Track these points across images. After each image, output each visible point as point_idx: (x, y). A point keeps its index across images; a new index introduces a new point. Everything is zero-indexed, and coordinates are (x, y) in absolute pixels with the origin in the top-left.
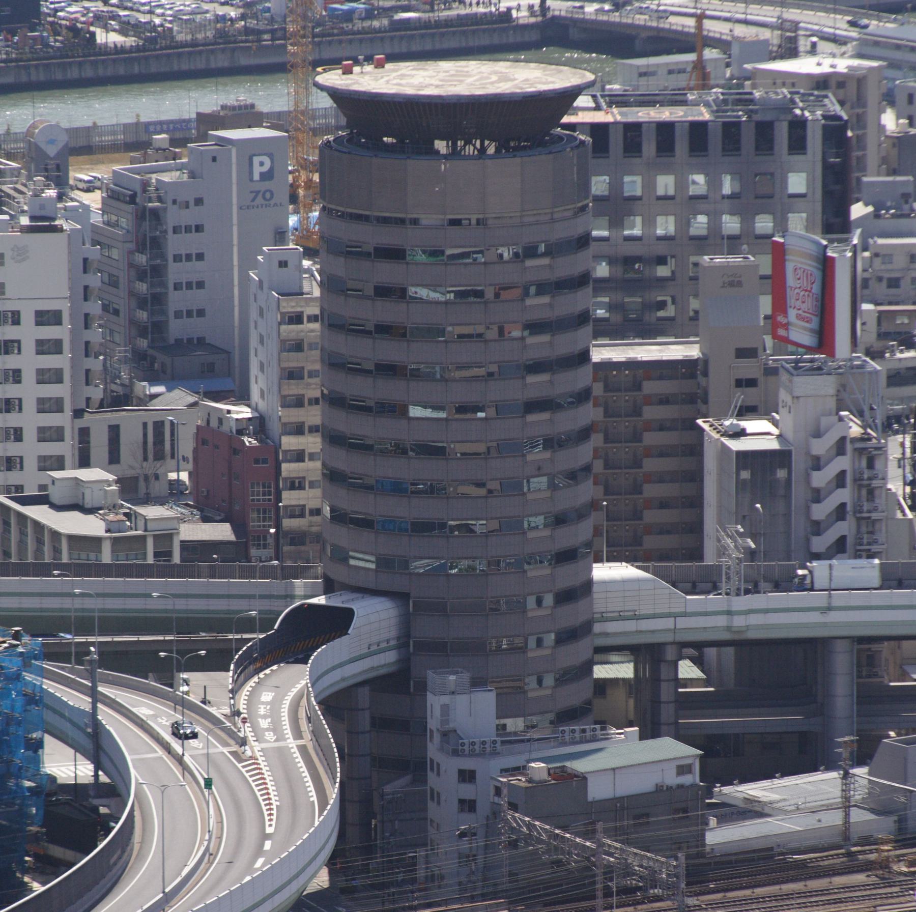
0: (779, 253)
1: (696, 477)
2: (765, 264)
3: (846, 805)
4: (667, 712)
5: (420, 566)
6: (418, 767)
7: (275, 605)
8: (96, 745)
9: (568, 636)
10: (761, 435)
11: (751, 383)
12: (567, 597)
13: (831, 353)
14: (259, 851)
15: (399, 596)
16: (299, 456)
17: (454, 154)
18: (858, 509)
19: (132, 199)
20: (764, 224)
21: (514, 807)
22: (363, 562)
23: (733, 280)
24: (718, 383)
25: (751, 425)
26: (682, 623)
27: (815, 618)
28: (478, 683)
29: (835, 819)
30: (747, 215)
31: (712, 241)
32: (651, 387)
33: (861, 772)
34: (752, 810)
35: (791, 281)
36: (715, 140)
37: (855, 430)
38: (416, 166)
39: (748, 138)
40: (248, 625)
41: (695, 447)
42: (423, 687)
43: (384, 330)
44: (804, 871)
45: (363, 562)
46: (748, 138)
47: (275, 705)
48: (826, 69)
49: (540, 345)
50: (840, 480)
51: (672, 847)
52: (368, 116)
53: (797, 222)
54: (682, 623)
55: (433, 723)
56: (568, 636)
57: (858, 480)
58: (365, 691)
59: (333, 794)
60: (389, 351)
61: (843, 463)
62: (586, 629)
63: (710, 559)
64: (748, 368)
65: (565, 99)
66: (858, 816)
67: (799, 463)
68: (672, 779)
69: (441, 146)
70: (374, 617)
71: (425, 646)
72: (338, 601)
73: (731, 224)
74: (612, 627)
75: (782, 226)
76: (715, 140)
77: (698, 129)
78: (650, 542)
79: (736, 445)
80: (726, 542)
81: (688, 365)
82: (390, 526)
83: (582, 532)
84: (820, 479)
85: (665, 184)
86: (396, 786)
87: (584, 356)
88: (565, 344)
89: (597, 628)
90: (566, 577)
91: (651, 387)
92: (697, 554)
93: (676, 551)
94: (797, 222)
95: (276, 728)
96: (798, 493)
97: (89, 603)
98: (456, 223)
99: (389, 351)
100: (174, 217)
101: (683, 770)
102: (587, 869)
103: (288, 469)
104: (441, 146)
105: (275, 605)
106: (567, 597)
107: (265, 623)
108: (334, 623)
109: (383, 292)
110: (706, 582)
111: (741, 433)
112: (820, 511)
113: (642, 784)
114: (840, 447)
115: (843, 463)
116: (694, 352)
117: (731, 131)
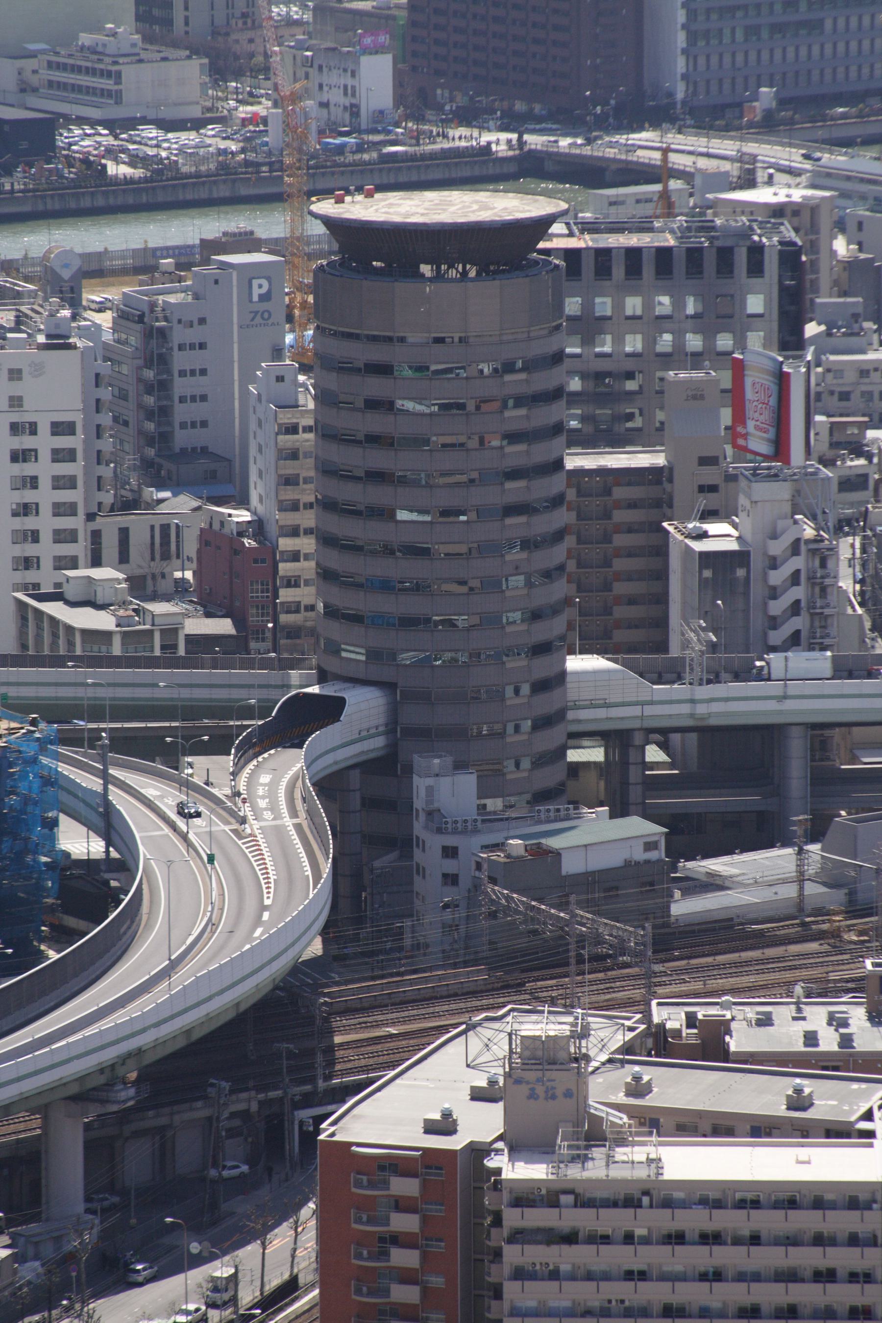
0: (739, 368)
1: (662, 575)
2: (725, 379)
3: (801, 879)
4: (635, 793)
5: (406, 658)
6: (405, 844)
7: (272, 694)
8: (108, 824)
9: (544, 723)
10: (721, 536)
11: (713, 489)
12: (542, 686)
13: (787, 461)
14: (258, 922)
15: (388, 686)
16: (295, 556)
18: (811, 605)
19: (141, 319)
21: (493, 880)
22: (354, 654)
23: (696, 393)
24: (682, 489)
25: (713, 528)
26: (649, 710)
27: (772, 705)
28: (460, 766)
29: (790, 891)
30: (709, 334)
31: (677, 357)
34: (714, 884)
35: (749, 394)
36: (680, 264)
37: (809, 532)
38: (403, 288)
40: (248, 712)
41: (660, 548)
42: (409, 770)
43: (373, 439)
44: (761, 940)
45: (354, 654)
46: (710, 262)
47: (273, 786)
48: (781, 198)
49: (517, 454)
51: (639, 917)
53: (755, 340)
54: (649, 710)
57: (811, 578)
60: (379, 459)
61: (798, 563)
62: (560, 716)
63: (675, 651)
64: (709, 476)
65: (540, 226)
67: (757, 563)
68: (639, 855)
69: (426, 269)
70: (364, 706)
71: (409, 732)
72: (330, 690)
73: (694, 342)
74: (584, 714)
75: (741, 344)
76: (680, 264)
77: (663, 254)
78: (620, 636)
79: (698, 546)
81: (653, 474)
83: (557, 626)
84: (777, 577)
85: (633, 304)
86: (385, 861)
87: (558, 464)
88: (540, 453)
89: (571, 715)
90: (542, 668)
91: (620, 493)
92: (662, 646)
93: (642, 642)
94: (755, 340)
95: (273, 808)
96: (757, 591)
97: (101, 693)
98: (439, 340)
99: (379, 459)
100: (179, 335)
101: (650, 846)
103: (285, 568)
104: (426, 269)
105: (272, 694)
106: (542, 686)
107: (264, 711)
108: (328, 710)
109: (372, 404)
111: (703, 535)
112: (777, 607)
113: (613, 859)
114: (795, 547)
115: (798, 563)
116: (659, 460)
117: (694, 256)
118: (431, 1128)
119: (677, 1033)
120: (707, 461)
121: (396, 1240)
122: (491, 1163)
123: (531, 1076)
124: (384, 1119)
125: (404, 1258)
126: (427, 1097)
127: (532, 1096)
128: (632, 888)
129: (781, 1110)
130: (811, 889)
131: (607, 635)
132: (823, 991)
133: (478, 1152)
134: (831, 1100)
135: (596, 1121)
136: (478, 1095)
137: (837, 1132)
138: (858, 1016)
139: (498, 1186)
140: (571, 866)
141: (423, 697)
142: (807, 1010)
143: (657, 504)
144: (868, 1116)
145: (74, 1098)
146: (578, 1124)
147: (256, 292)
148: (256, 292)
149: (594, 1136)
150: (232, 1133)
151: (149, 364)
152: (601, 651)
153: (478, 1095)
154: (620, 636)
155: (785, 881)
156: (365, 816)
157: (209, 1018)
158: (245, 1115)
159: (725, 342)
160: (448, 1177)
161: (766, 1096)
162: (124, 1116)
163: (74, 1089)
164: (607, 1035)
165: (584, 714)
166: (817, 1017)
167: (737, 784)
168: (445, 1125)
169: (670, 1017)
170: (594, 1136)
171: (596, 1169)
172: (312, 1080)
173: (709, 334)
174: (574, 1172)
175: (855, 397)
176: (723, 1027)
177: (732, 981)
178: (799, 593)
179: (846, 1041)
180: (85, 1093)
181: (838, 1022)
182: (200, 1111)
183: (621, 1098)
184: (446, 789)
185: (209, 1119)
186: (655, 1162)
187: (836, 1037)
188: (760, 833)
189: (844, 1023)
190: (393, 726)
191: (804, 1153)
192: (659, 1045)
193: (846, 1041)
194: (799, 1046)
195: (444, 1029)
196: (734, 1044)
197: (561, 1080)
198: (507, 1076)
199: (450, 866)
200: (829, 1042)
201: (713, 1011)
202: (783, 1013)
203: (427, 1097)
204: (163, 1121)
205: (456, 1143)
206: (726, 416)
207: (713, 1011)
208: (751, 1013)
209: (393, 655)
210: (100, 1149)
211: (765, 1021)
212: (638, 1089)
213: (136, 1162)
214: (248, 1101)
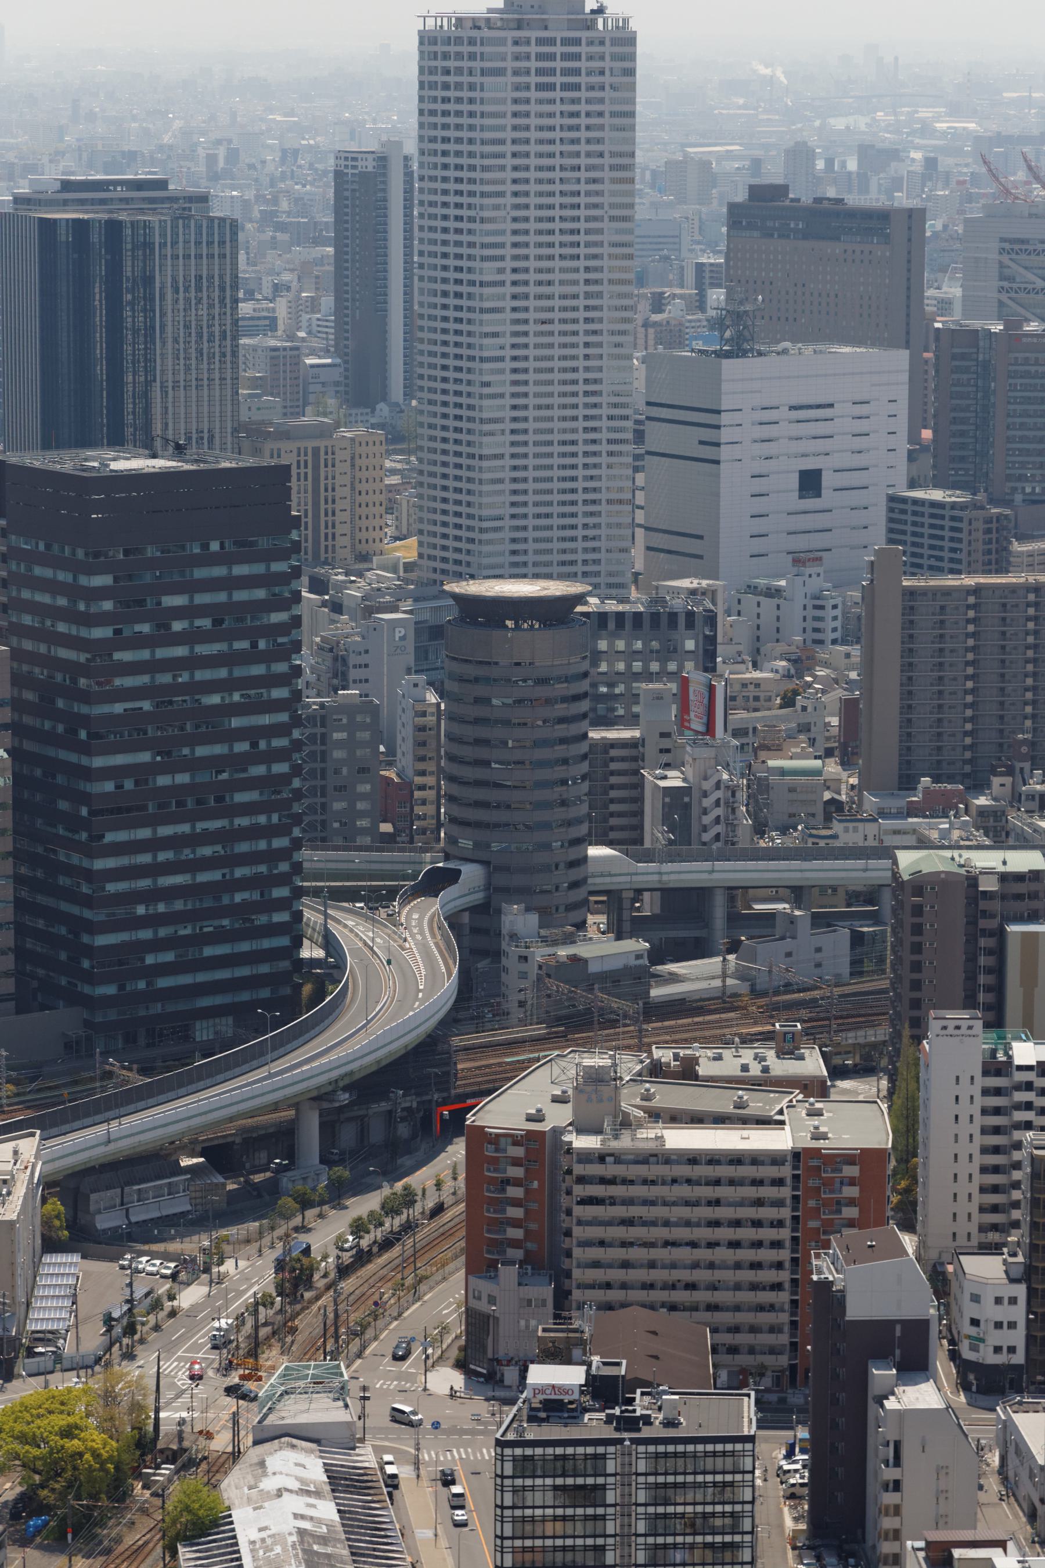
0: (685, 683)
1: (640, 800)
2: (673, 687)
3: (724, 976)
4: (627, 926)
5: (495, 846)
6: (497, 955)
7: (417, 867)
8: (329, 942)
9: (575, 885)
10: (674, 780)
11: (668, 751)
12: (573, 864)
13: (713, 735)
14: (416, 999)
15: (485, 863)
16: (422, 788)
17: (517, 627)
18: (727, 819)
19: (331, 650)
20: (672, 667)
21: (549, 976)
22: (466, 843)
23: (659, 697)
24: (650, 751)
25: (670, 773)
26: (635, 878)
27: (705, 876)
28: (528, 910)
29: (718, 983)
30: (663, 661)
31: (648, 676)
32: (613, 753)
33: (731, 957)
34: (674, 978)
35: (692, 697)
36: (646, 622)
37: (725, 776)
38: (497, 634)
39: (664, 621)
40: (405, 878)
41: (639, 785)
42: (499, 912)
43: (477, 721)
44: (700, 1011)
45: (466, 843)
46: (664, 621)
47: (420, 921)
48: (695, 585)
49: (561, 731)
50: (717, 803)
51: (635, 998)
52: (471, 606)
53: (689, 665)
54: (635, 878)
55: (504, 931)
56: (575, 885)
57: (727, 803)
58: (467, 914)
59: (455, 971)
60: (482, 732)
61: (719, 794)
62: (584, 881)
63: (647, 844)
64: (666, 743)
65: (580, 599)
66: (730, 982)
67: (695, 794)
68: (633, 962)
69: (510, 623)
70: (471, 874)
71: (499, 890)
72: (451, 865)
73: (655, 667)
74: (598, 880)
75: (681, 667)
76: (646, 622)
77: (637, 615)
78: (613, 835)
79: (663, 784)
80: (655, 833)
81: (633, 744)
82: (478, 825)
83: (583, 829)
84: (707, 802)
85: (621, 645)
86: (483, 965)
87: (585, 736)
88: (574, 729)
89: (590, 881)
90: (573, 854)
91: (613, 753)
92: (641, 841)
93: (630, 839)
94: (689, 665)
95: (421, 932)
96: (695, 811)
97: (321, 865)
98: (518, 664)
99: (482, 732)
100: (353, 660)
101: (638, 957)
102: (588, 1011)
103: (417, 794)
104: (510, 623)
105: (417, 867)
106: (573, 864)
107: (414, 877)
108: (451, 877)
109: (478, 701)
110: (647, 857)
111: (665, 778)
112: (706, 820)
113: (617, 964)
114: (718, 785)
115: (719, 794)
116: (637, 734)
117: (655, 617)
118: (530, 1118)
119: (668, 1064)
120: (664, 735)
121: (507, 1182)
122: (566, 1138)
123: (588, 1089)
124: (502, 1113)
125: (515, 1192)
126: (528, 1100)
127: (589, 1100)
128: (632, 979)
129: (730, 1109)
130: (730, 982)
131: (606, 835)
132: (747, 1040)
133: (558, 1132)
134: (757, 1103)
135: (626, 1115)
136: (556, 1100)
137: (763, 1122)
138: (771, 1054)
139: (569, 1151)
140: (593, 968)
141: (506, 869)
142: (742, 1052)
143: (635, 759)
144: (781, 1112)
145: (314, 1099)
146: (615, 1117)
147: (397, 636)
148: (397, 636)
149: (626, 1123)
150: (403, 1119)
151: (335, 676)
152: (610, 844)
153: (556, 1100)
154: (613, 835)
155: (713, 978)
156: (476, 939)
157: (390, 1053)
158: (409, 1109)
159: (672, 667)
160: (538, 1147)
161: (722, 1102)
162: (341, 1109)
163: (314, 1094)
164: (629, 1065)
165: (598, 880)
166: (747, 1056)
167: (683, 922)
168: (538, 1117)
169: (664, 1055)
170: (626, 1123)
171: (624, 1142)
172: (448, 1090)
173: (663, 661)
174: (614, 1144)
175: (740, 699)
176: (694, 1061)
177: (698, 1034)
178: (719, 811)
179: (766, 1070)
180: (320, 1097)
181: (759, 1059)
182: (384, 1106)
183: (638, 1101)
184: (517, 919)
185: (390, 1112)
186: (660, 1139)
187: (759, 1067)
188: (698, 950)
189: (764, 1059)
190: (488, 886)
191: (745, 1133)
192: (656, 1070)
193: (766, 1070)
194: (739, 1073)
195: (538, 1060)
196: (702, 1070)
197: (606, 1091)
198: (576, 1088)
199: (523, 967)
200: (755, 1070)
201: (688, 1052)
202: (727, 1054)
203: (528, 1100)
204: (362, 1113)
205: (546, 1127)
206: (674, 710)
207: (688, 1052)
208: (710, 1053)
209: (488, 846)
210: (328, 1129)
211: (719, 1058)
212: (647, 1097)
213: (348, 1136)
214: (411, 1102)
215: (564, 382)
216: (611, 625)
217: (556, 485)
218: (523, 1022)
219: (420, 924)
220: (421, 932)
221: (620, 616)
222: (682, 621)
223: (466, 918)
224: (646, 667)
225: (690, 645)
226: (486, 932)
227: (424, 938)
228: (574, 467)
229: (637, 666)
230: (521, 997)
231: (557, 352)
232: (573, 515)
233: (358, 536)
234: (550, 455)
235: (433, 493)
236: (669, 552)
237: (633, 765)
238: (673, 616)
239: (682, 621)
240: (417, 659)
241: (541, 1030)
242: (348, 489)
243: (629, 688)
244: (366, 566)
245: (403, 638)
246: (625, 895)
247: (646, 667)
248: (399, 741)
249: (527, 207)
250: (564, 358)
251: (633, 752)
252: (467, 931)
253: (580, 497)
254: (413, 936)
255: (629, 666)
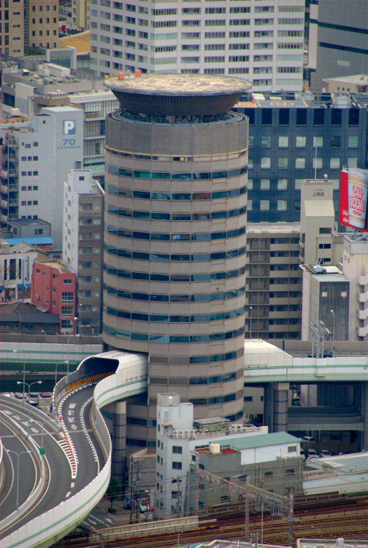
0: (344, 179)
20: (335, 163)
26: (290, 371)
30: (326, 158)
32: (275, 247)
35: (351, 193)
36: (310, 118)
39: (328, 118)
42: (154, 402)
46: (328, 118)
47: (77, 410)
54: (290, 371)
62: (241, 371)
71: (156, 381)
76: (310, 118)
78: (273, 328)
85: (283, 141)
86: (139, 455)
88: (229, 346)
89: (246, 373)
91: (275, 247)
92: (296, 335)
93: (283, 329)
100: (22, 152)
147: (67, 129)
148: (67, 129)
152: (268, 336)
154: (273, 328)
159: (335, 163)
173: (326, 158)
184: (175, 413)
190: (145, 377)
215: (236, 35)
216: (275, 120)
217: (228, 53)
218: (176, 512)
219: (76, 415)
220: (77, 423)
221: (284, 113)
222: (345, 118)
223: (122, 409)
224: (309, 164)
225: (353, 142)
226: (142, 422)
227: (80, 427)
228: (245, 34)
229: (300, 163)
230: (175, 487)
231: (228, 28)
232: (245, 46)
233: (32, 40)
234: (222, 47)
235: (106, 33)
236: (339, 27)
237: (293, 260)
238: (337, 113)
239: (345, 118)
240: (86, 152)
241: (192, 523)
242: (22, 41)
243: (291, 184)
244: (40, 58)
245: (72, 132)
246: (281, 387)
247: (309, 164)
248: (65, 233)
249: (196, 59)
250: (235, 47)
251: (293, 247)
252: (123, 421)
253: (252, 28)
254: (68, 425)
255: (292, 163)
